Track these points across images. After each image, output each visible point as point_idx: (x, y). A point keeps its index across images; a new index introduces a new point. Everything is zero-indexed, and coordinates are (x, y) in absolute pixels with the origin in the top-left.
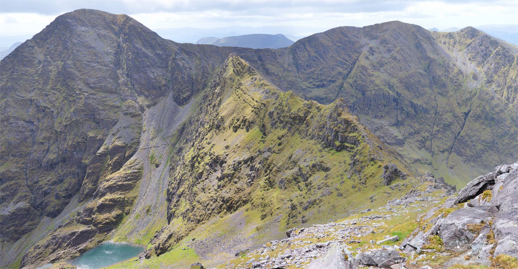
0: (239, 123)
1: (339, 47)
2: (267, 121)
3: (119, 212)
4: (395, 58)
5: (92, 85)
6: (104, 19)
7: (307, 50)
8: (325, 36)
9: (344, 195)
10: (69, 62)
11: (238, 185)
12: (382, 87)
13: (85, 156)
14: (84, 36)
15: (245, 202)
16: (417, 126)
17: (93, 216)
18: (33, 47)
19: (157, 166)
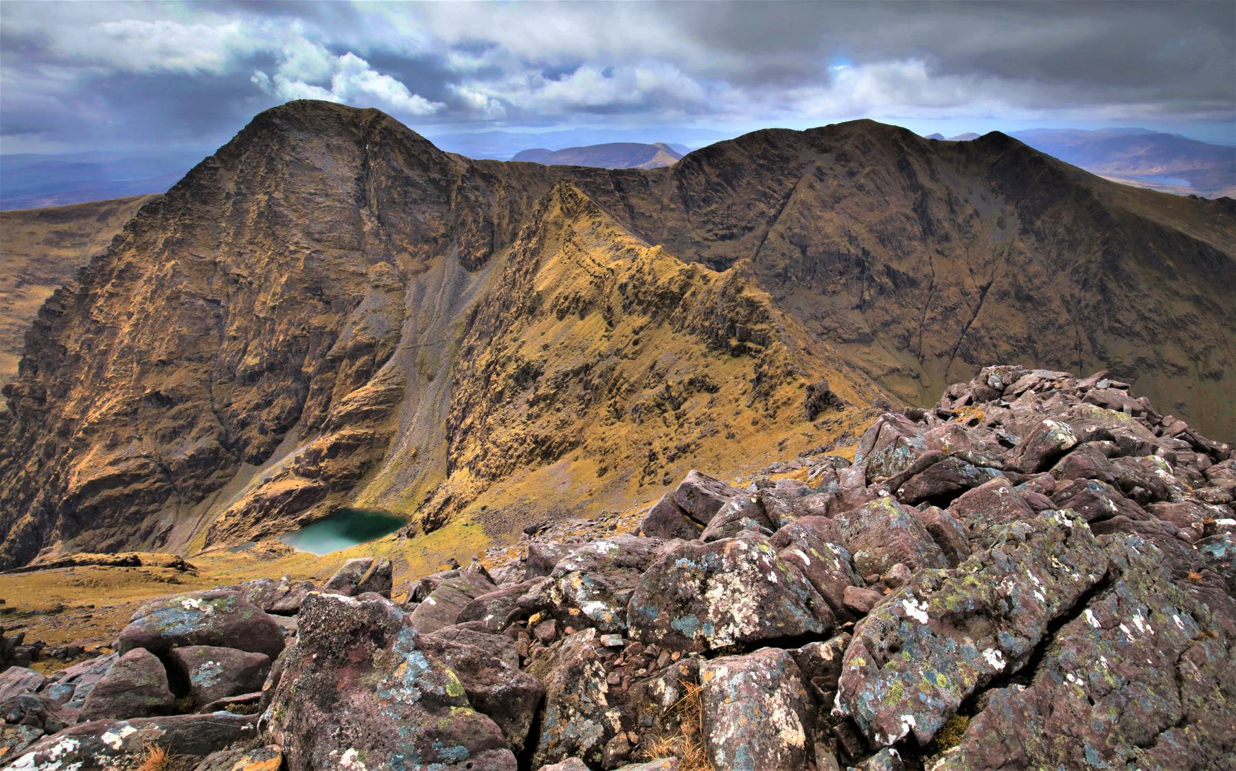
0: (567, 304)
1: (761, 166)
2: (616, 300)
3: (364, 458)
4: (861, 188)
5: (317, 236)
6: (339, 117)
7: (704, 172)
8: (737, 147)
9: (738, 437)
10: (276, 195)
11: (562, 415)
12: (836, 239)
13: (306, 362)
14: (304, 148)
15: (574, 445)
16: (896, 310)
17: (322, 464)
18: (217, 169)
19: (431, 379)
